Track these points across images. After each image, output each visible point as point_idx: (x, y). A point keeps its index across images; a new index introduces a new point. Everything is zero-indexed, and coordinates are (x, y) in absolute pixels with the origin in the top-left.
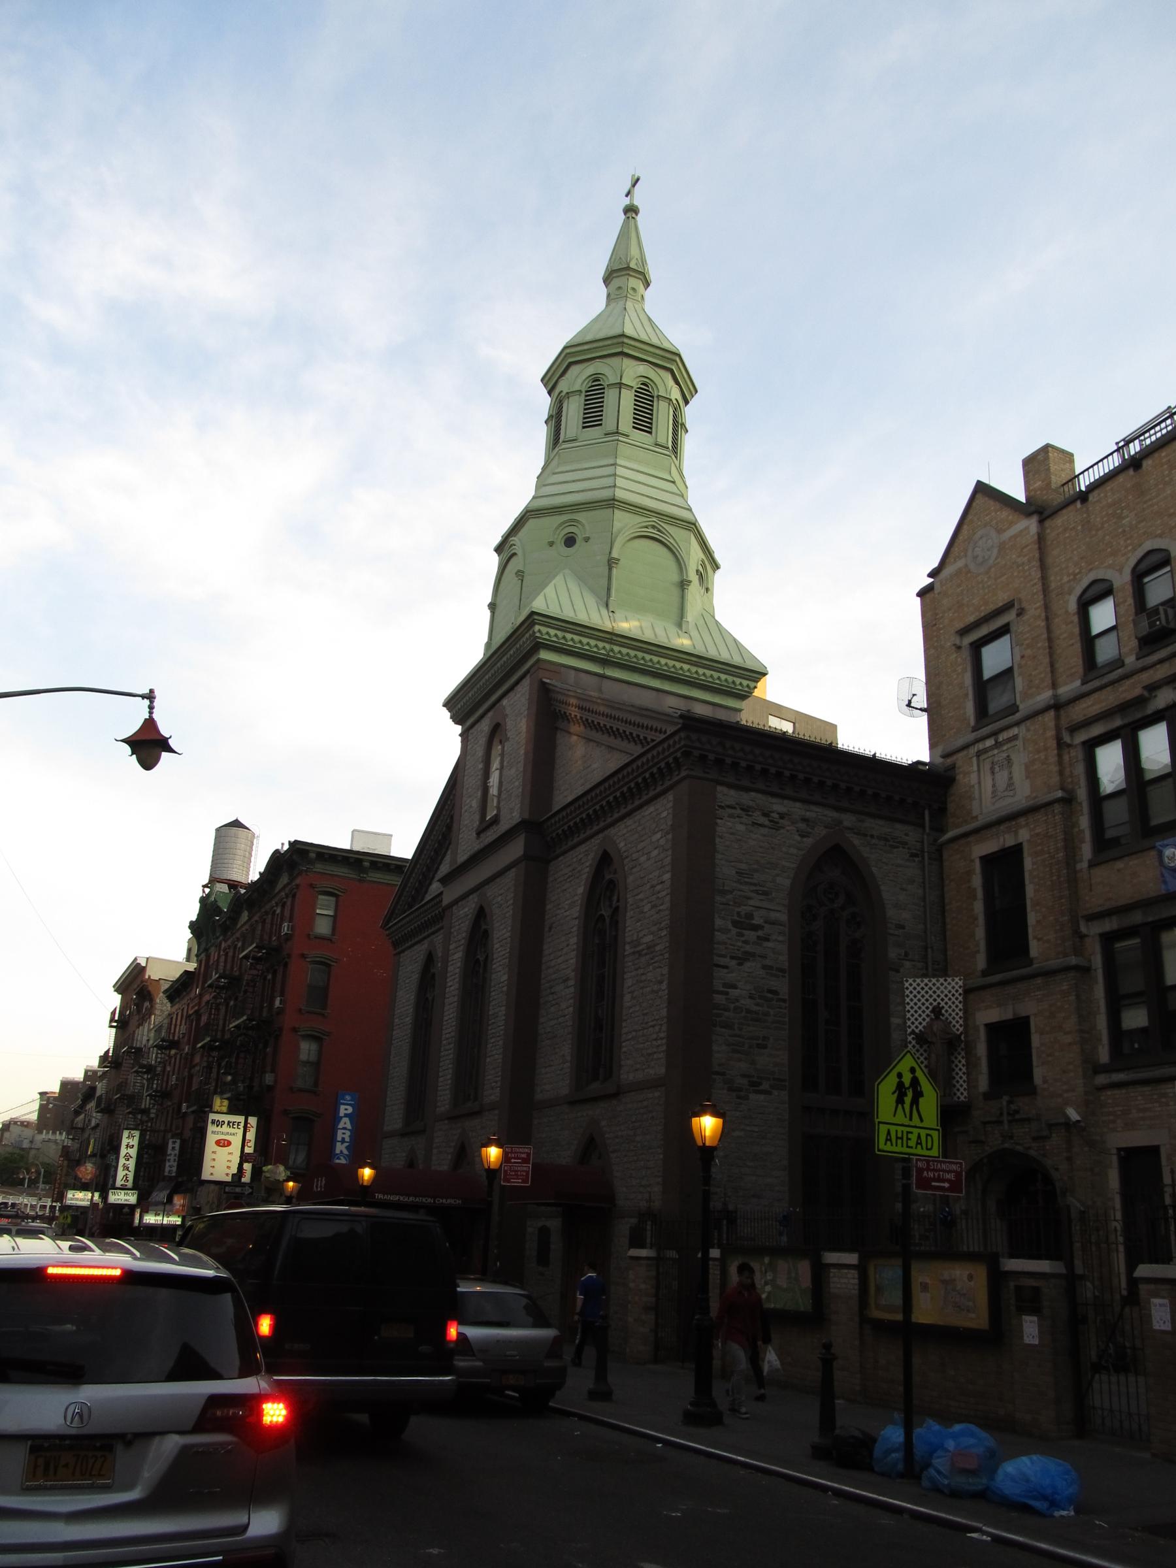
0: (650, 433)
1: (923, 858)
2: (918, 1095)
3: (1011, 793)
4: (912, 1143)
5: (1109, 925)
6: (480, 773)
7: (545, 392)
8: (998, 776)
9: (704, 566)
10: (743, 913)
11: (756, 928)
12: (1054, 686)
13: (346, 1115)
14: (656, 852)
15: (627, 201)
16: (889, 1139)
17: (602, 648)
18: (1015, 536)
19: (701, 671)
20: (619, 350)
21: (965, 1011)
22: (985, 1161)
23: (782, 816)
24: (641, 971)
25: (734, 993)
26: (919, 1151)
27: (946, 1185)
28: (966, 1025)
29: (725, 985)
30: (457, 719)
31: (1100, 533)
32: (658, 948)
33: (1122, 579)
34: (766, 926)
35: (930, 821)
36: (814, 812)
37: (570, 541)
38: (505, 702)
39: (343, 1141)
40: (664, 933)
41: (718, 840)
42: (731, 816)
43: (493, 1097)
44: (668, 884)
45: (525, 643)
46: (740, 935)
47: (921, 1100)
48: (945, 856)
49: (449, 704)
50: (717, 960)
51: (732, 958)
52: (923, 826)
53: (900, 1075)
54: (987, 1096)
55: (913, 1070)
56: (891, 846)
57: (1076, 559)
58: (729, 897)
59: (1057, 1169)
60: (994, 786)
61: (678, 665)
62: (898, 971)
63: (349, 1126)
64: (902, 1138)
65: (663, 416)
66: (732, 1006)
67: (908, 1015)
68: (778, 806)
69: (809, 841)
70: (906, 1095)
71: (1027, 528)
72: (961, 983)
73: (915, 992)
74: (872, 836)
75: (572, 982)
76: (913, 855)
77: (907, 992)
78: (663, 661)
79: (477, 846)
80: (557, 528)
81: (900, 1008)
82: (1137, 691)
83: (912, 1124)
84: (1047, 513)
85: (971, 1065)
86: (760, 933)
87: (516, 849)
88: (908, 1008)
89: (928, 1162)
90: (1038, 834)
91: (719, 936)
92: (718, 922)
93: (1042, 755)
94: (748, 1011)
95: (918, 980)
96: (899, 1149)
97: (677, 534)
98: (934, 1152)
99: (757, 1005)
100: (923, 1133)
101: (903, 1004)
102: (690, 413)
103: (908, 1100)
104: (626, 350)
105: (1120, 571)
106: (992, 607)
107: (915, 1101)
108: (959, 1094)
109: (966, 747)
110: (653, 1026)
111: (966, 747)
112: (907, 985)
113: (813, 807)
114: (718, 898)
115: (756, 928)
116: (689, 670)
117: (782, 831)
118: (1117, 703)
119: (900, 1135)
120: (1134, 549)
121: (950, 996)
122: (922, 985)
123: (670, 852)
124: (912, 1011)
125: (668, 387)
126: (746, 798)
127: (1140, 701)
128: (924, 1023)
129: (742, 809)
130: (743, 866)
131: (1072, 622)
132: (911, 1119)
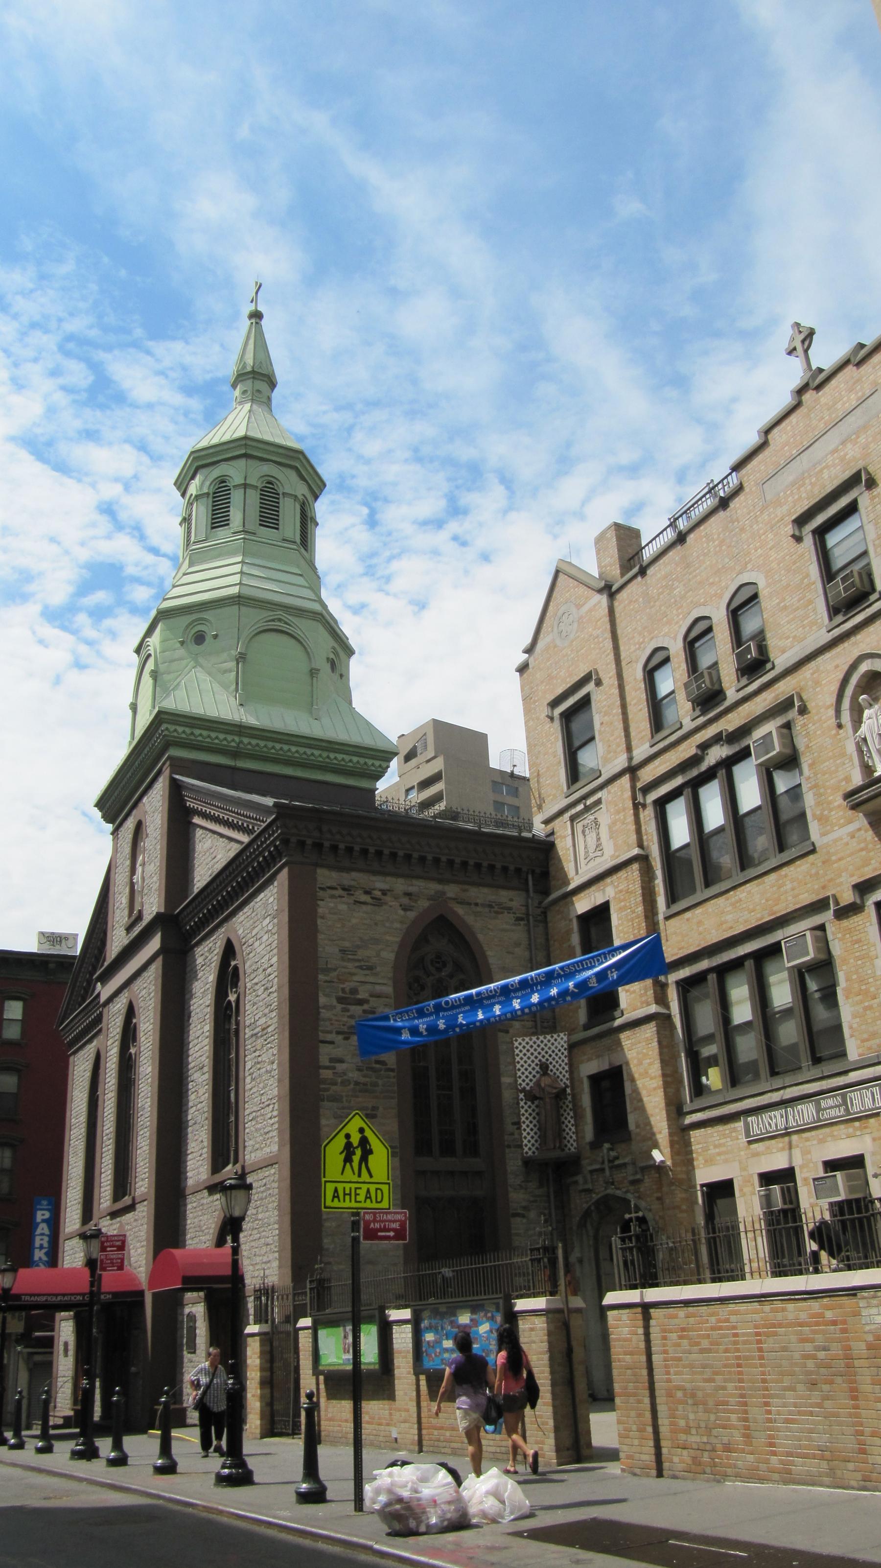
0: (277, 529)
1: (528, 921)
2: (367, 1152)
3: (599, 853)
4: (361, 1198)
5: (685, 973)
6: (128, 869)
7: (178, 494)
8: (588, 839)
9: (336, 653)
10: (347, 990)
11: (360, 1002)
12: (629, 749)
13: (43, 1221)
14: (265, 937)
15: (252, 307)
16: (336, 1195)
17: (233, 741)
18: (591, 610)
19: (332, 756)
20: (243, 452)
21: (571, 1064)
22: (593, 1208)
23: (384, 892)
24: (257, 1053)
25: (340, 1067)
26: (368, 1204)
27: (392, 1234)
28: (572, 1079)
29: (332, 1060)
30: (109, 817)
31: (657, 603)
32: (269, 1030)
33: (677, 648)
34: (371, 999)
35: (534, 885)
36: (417, 886)
37: (200, 638)
38: (145, 800)
39: (41, 1247)
40: (274, 1014)
41: (319, 921)
42: (333, 897)
43: (143, 1189)
44: (276, 965)
45: (157, 741)
46: (345, 1010)
47: (370, 1157)
48: (549, 918)
49: (100, 804)
50: (322, 1036)
51: (338, 1033)
52: (527, 891)
53: (348, 1136)
54: (595, 1145)
55: (361, 1130)
56: (497, 913)
57: (640, 628)
58: (334, 974)
59: (650, 1210)
60: (585, 848)
61: (309, 751)
62: (507, 1032)
63: (47, 1231)
64: (350, 1194)
65: (289, 513)
66: (339, 1080)
67: (519, 1074)
68: (380, 883)
69: (412, 915)
70: (354, 1154)
71: (599, 602)
72: (565, 1038)
73: (524, 1051)
74: (476, 904)
75: (206, 1069)
76: (519, 919)
77: (517, 1051)
78: (294, 749)
79: (126, 942)
80: (187, 627)
81: (511, 1067)
82: (693, 751)
83: (360, 1180)
84: (614, 588)
85: (578, 1117)
86: (366, 1007)
87: (155, 944)
88: (518, 1066)
89: (375, 1214)
90: (621, 891)
91: (324, 1014)
92: (322, 1000)
93: (621, 816)
94: (357, 1083)
95: (527, 1039)
96: (347, 1204)
97: (303, 627)
98: (385, 1204)
99: (364, 1076)
100: (373, 1188)
101: (514, 1063)
102: (321, 508)
103: (356, 1158)
104: (249, 452)
105: (675, 639)
106: (576, 678)
107: (364, 1159)
108: (569, 1145)
109: (561, 813)
110: (269, 1105)
111: (561, 813)
112: (516, 1044)
113: (415, 882)
114: (321, 977)
115: (360, 1002)
116: (320, 756)
117: (385, 907)
118: (678, 762)
119: (347, 1191)
120: (684, 618)
121: (556, 1051)
122: (531, 1043)
123: (276, 936)
124: (523, 1070)
125: (289, 483)
126: (347, 878)
127: (694, 761)
128: (534, 1080)
129: (344, 889)
130: (347, 944)
131: (640, 688)
132: (359, 1175)
